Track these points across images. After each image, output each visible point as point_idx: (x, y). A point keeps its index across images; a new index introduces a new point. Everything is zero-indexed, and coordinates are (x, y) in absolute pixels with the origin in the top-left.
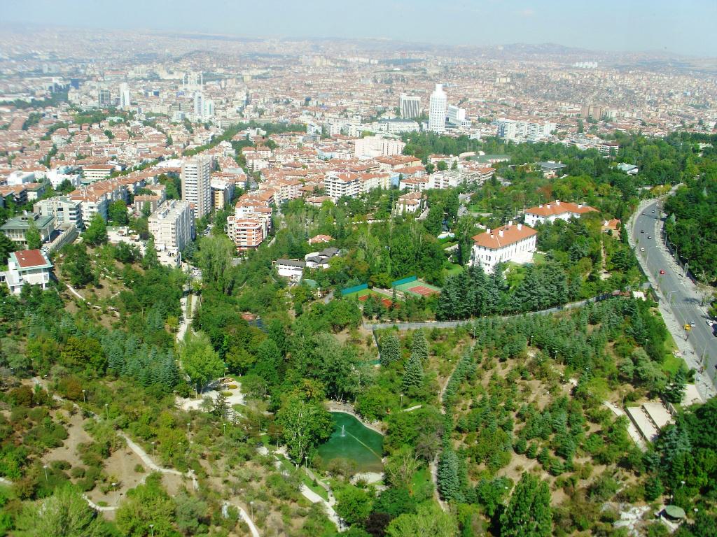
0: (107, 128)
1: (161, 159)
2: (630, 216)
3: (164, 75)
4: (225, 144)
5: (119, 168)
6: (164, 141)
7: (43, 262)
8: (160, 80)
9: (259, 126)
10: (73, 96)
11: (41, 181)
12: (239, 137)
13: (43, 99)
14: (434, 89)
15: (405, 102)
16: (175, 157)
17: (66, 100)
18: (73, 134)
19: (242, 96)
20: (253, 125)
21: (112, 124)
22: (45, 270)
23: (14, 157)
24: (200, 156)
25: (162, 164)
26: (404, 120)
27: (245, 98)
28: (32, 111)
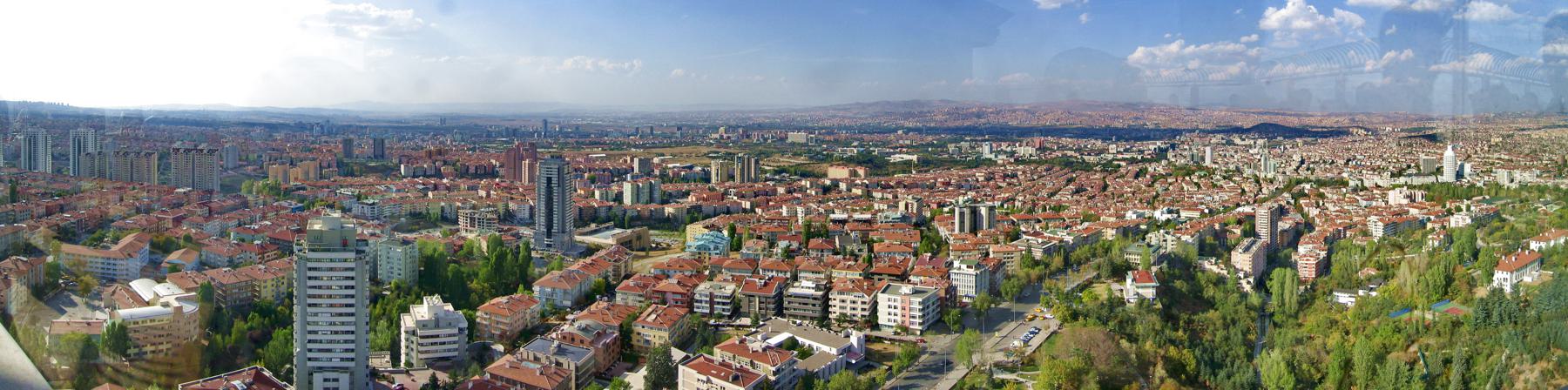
0: (1196, 180)
1: (1238, 205)
2: (975, 328)
3: (1237, 141)
4: (1286, 195)
5: (1207, 211)
6: (1240, 191)
7: (1151, 281)
8: (1235, 145)
9: (1311, 181)
10: (1170, 155)
11: (1149, 218)
12: (1296, 189)
13: (1149, 157)
14: (1446, 148)
15: (1424, 160)
16: (1248, 203)
17: (1166, 158)
18: (1170, 184)
19: (1297, 158)
20: (1308, 181)
21: (1200, 177)
22: (1153, 287)
23: (1128, 198)
24: (1269, 204)
25: (1240, 209)
26: (1424, 175)
27: (1300, 159)
28: (1141, 165)
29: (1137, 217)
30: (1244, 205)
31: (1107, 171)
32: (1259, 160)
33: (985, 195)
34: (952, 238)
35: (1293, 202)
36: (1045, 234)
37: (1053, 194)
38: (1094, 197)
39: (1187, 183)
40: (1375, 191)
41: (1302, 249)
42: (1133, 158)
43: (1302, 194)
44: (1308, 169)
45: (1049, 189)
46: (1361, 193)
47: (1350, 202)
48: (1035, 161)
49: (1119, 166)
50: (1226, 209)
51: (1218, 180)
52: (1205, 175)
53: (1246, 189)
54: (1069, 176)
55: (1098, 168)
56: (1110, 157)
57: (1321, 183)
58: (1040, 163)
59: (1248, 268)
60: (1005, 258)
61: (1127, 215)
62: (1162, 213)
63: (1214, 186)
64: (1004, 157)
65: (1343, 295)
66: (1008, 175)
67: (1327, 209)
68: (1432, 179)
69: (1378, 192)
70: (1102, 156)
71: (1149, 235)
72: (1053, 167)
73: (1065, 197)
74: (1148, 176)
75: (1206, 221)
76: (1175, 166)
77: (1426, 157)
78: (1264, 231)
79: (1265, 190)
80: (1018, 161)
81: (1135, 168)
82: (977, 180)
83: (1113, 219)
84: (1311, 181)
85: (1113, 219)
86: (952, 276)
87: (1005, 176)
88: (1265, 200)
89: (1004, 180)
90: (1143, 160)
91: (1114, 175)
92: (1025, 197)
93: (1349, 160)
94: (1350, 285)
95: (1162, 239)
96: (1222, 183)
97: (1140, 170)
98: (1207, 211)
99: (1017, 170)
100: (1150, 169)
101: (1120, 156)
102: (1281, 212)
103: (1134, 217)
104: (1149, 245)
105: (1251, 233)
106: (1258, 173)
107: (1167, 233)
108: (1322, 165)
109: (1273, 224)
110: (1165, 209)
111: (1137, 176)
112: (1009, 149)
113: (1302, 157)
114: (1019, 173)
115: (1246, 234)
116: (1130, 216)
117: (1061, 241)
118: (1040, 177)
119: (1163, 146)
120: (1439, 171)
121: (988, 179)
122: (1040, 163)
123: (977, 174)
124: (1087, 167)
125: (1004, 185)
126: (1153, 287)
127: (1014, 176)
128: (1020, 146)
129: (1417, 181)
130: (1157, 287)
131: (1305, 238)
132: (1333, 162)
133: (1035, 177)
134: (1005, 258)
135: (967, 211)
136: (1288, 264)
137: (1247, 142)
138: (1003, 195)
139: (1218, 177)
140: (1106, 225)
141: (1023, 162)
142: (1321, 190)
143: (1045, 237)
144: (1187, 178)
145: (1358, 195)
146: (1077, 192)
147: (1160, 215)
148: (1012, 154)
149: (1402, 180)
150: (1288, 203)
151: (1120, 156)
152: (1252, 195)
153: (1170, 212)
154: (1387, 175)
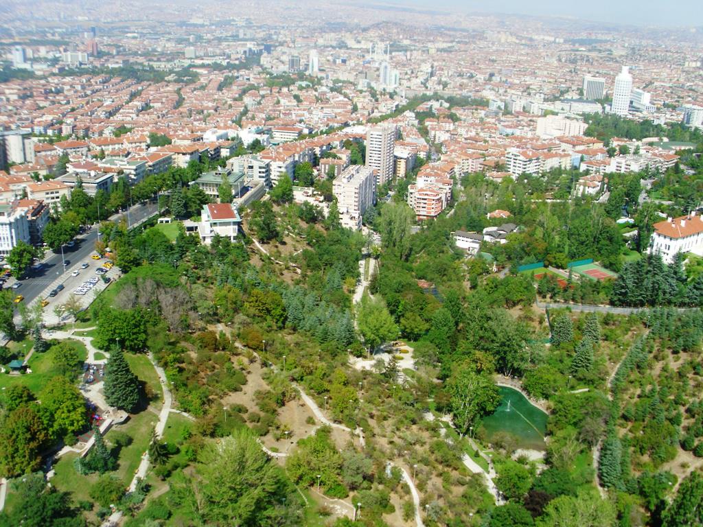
0: (296, 92)
1: (346, 125)
3: (351, 43)
5: (306, 131)
6: (350, 107)
7: (233, 216)
10: (265, 60)
11: (233, 139)
12: (422, 107)
13: (237, 62)
16: (359, 123)
17: (259, 64)
18: (263, 97)
19: (426, 68)
20: (437, 97)
21: (301, 88)
24: (385, 124)
25: (347, 130)
26: (587, 101)
27: (430, 70)
28: (227, 73)
30: (354, 125)
31: (182, 81)
33: (20, 119)
36: (100, 165)
37: (111, 114)
42: (215, 63)
43: (429, 114)
45: (107, 106)
48: (86, 72)
50: (331, 130)
52: (308, 86)
54: (133, 89)
55: (171, 77)
56: (186, 63)
58: (94, 72)
60: (48, 198)
66: (51, 91)
70: (176, 61)
72: (111, 78)
73: (127, 116)
75: (303, 143)
76: (271, 74)
80: (63, 72)
81: (219, 77)
82: (8, 100)
84: (442, 98)
87: (48, 93)
88: (383, 118)
89: (46, 98)
90: (234, 67)
91: (192, 86)
99: (64, 84)
105: (359, 156)
112: (50, 56)
118: (94, 92)
119: (255, 49)
121: (24, 97)
122: (94, 72)
123: (7, 91)
124: (158, 77)
125: (46, 104)
127: (59, 92)
128: (65, 50)
131: (426, 169)
132: (471, 77)
133: (89, 92)
134: (48, 198)
137: (364, 45)
138: (44, 118)
141: (71, 73)
144: (285, 90)
147: (247, 137)
148: (55, 61)
149: (557, 106)
151: (199, 62)
152: (366, 113)
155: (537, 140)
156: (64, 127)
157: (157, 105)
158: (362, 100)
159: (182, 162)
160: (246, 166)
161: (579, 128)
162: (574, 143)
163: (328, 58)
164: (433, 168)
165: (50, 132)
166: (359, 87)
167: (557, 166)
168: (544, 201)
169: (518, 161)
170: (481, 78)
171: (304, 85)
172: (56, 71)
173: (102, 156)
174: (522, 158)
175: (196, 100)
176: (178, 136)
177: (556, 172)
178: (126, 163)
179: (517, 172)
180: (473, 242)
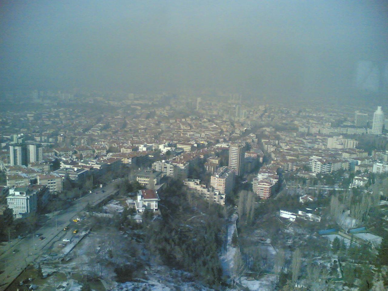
0: (189, 122)
1: (218, 142)
9: (271, 126)
13: (157, 103)
18: (171, 124)
21: (192, 120)
25: (219, 145)
29: (147, 149)
32: (235, 108)
34: (8, 170)
35: (256, 140)
38: (116, 132)
39: (184, 124)
40: (318, 137)
41: (260, 177)
44: (269, 117)
46: (307, 138)
47: (298, 143)
49: (137, 109)
51: (205, 122)
53: (224, 130)
57: (278, 129)
59: (222, 189)
60: (49, 183)
61: (140, 148)
62: (165, 146)
63: (201, 126)
64: (49, 101)
65: (285, 212)
67: (281, 147)
68: (363, 131)
69: (320, 137)
71: (155, 164)
74: (156, 118)
77: (360, 114)
78: (234, 161)
79: (238, 131)
83: (129, 151)
85: (129, 151)
86: (9, 201)
92: (66, 132)
93: (300, 111)
94: (293, 207)
95: (163, 166)
96: (206, 124)
97: (151, 113)
98: (195, 145)
100: (158, 113)
101: (136, 102)
102: (248, 148)
103: (145, 149)
104: (154, 171)
106: (233, 118)
107: (167, 162)
108: (280, 115)
109: (241, 155)
110: (166, 144)
111: (148, 117)
113: (265, 107)
114: (61, 114)
115: (221, 164)
116: (142, 148)
117: (91, 168)
120: (369, 126)
123: (28, 115)
125: (50, 123)
126: (156, 201)
129: (351, 131)
130: (158, 202)
133: (73, 117)
134: (49, 183)
135: (18, 149)
136: (248, 187)
139: (205, 120)
140: (124, 155)
141: (51, 263)
142: (278, 133)
143: (79, 166)
144: (183, 120)
145: (305, 139)
146: (105, 128)
150: (253, 141)
151: (136, 102)
152: (228, 134)
153: (169, 145)
154: (328, 124)
155: (328, 151)
156: (59, 137)
157: (113, 126)
158: (226, 126)
159: (127, 161)
160: (163, 167)
161: (351, 144)
162: (350, 152)
163: (208, 102)
164: (268, 168)
165: (51, 140)
166: (224, 119)
167: (339, 168)
168: (334, 189)
169: (317, 165)
170: (293, 113)
171: (194, 118)
172: (55, 104)
173: (81, 157)
174: (319, 163)
175: (134, 124)
176: (124, 147)
177: (341, 171)
178: (95, 163)
179: (317, 171)
180: (292, 214)
